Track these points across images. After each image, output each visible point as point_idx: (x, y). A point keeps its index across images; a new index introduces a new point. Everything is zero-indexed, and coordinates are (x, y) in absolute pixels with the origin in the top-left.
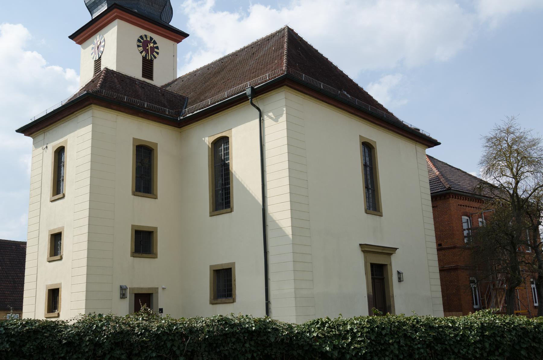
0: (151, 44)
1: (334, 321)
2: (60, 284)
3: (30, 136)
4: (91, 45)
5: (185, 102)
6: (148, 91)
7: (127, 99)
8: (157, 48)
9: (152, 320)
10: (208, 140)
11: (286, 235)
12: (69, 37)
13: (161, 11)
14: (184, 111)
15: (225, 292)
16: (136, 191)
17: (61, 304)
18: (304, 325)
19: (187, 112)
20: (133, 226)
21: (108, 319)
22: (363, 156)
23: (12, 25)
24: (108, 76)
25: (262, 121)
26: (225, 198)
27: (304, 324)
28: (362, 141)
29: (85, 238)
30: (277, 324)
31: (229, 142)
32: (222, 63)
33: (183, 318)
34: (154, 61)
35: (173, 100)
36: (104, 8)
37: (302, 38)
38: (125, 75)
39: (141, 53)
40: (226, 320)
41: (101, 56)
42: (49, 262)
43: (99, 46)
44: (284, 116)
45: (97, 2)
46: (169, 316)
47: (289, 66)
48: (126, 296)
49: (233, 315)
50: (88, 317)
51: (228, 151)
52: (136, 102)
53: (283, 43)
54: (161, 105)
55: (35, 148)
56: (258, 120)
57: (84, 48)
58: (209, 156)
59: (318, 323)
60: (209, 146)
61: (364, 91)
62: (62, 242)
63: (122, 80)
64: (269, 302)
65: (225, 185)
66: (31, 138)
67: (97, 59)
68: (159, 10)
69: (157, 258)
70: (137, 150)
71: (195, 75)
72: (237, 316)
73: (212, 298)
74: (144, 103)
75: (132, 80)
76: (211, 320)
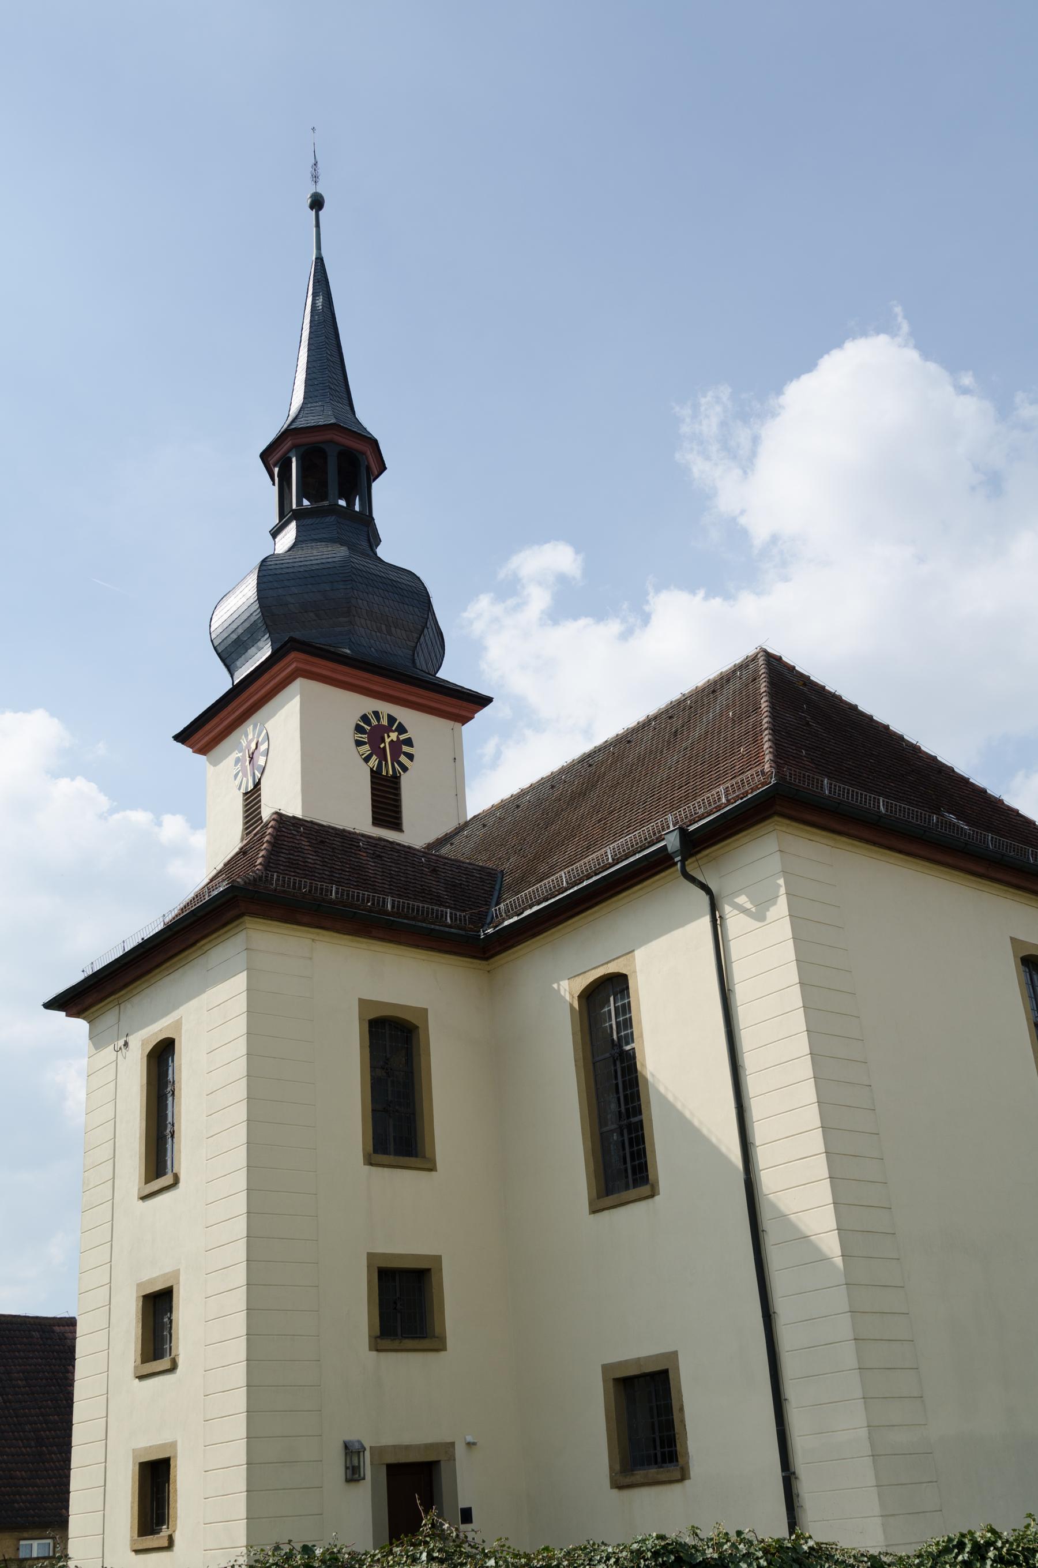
0: (391, 734)
1: (1011, 1539)
2: (173, 1445)
3: (84, 1015)
4: (231, 753)
5: (495, 885)
6: (393, 865)
7: (337, 893)
8: (409, 742)
9: (459, 1559)
10: (569, 987)
11: (826, 1259)
12: (173, 737)
13: (413, 644)
14: (496, 910)
15: (655, 1449)
16: (376, 1151)
17: (175, 1508)
18: (918, 1557)
19: (503, 914)
20: (371, 1256)
21: (329, 1560)
22: (1028, 999)
23: (20, 715)
24: (283, 834)
25: (718, 922)
26: (632, 1154)
27: (917, 1553)
28: (1022, 955)
29: (239, 1300)
30: (836, 1557)
31: (628, 988)
32: (590, 765)
33: (546, 1549)
34: (402, 778)
35: (461, 884)
36: (263, 652)
37: (808, 678)
38: (329, 827)
39: (367, 760)
40: (678, 1552)
41: (260, 780)
42: (141, 1378)
43: (253, 753)
44: (782, 902)
45: (245, 639)
46: (507, 1545)
47: (781, 759)
48: (362, 1475)
49: (698, 1531)
50: (274, 1555)
51: (628, 1016)
52: (363, 900)
53: (757, 694)
54: (431, 899)
55: (96, 1050)
56: (706, 921)
57: (215, 763)
58: (573, 1034)
59: (961, 1546)
60: (571, 1006)
61: (1008, 807)
62: (174, 1317)
63: (322, 842)
64: (794, 1473)
66: (85, 1022)
67: (249, 790)
68: (408, 642)
69: (444, 1349)
70: (370, 1032)
71: (518, 806)
72: (711, 1535)
73: (618, 1467)
74: (384, 898)
75: (347, 838)
76: (632, 1552)
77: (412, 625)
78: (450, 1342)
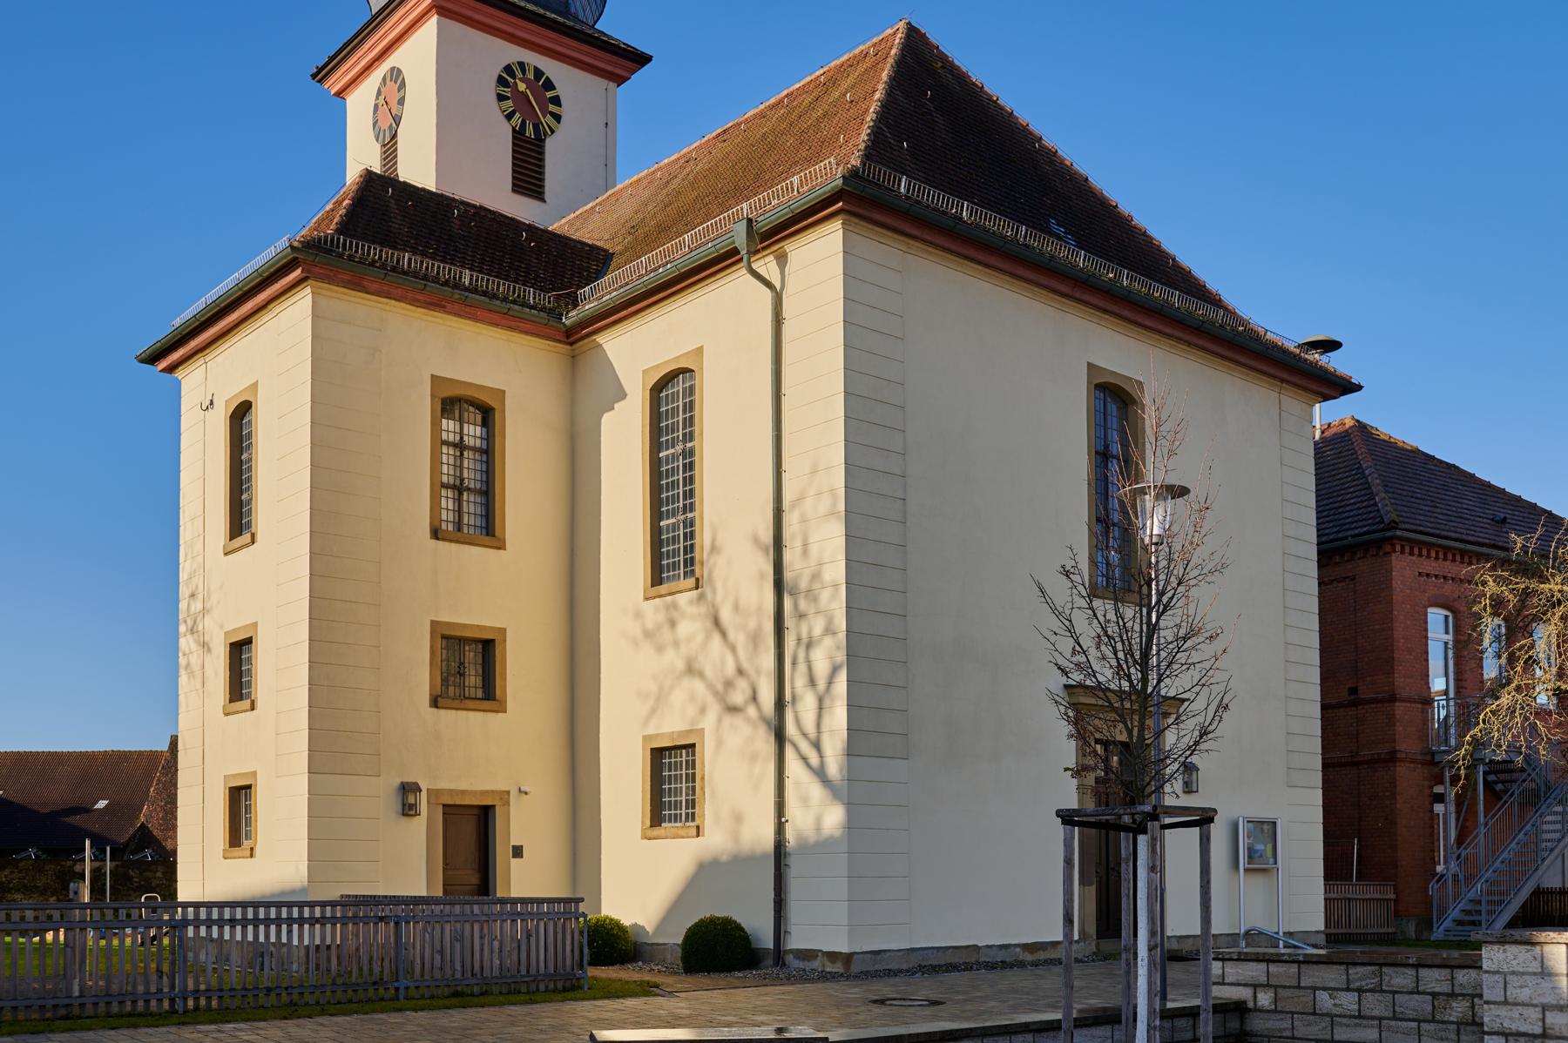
14: (581, 293)
42: (226, 714)
78: (510, 703)
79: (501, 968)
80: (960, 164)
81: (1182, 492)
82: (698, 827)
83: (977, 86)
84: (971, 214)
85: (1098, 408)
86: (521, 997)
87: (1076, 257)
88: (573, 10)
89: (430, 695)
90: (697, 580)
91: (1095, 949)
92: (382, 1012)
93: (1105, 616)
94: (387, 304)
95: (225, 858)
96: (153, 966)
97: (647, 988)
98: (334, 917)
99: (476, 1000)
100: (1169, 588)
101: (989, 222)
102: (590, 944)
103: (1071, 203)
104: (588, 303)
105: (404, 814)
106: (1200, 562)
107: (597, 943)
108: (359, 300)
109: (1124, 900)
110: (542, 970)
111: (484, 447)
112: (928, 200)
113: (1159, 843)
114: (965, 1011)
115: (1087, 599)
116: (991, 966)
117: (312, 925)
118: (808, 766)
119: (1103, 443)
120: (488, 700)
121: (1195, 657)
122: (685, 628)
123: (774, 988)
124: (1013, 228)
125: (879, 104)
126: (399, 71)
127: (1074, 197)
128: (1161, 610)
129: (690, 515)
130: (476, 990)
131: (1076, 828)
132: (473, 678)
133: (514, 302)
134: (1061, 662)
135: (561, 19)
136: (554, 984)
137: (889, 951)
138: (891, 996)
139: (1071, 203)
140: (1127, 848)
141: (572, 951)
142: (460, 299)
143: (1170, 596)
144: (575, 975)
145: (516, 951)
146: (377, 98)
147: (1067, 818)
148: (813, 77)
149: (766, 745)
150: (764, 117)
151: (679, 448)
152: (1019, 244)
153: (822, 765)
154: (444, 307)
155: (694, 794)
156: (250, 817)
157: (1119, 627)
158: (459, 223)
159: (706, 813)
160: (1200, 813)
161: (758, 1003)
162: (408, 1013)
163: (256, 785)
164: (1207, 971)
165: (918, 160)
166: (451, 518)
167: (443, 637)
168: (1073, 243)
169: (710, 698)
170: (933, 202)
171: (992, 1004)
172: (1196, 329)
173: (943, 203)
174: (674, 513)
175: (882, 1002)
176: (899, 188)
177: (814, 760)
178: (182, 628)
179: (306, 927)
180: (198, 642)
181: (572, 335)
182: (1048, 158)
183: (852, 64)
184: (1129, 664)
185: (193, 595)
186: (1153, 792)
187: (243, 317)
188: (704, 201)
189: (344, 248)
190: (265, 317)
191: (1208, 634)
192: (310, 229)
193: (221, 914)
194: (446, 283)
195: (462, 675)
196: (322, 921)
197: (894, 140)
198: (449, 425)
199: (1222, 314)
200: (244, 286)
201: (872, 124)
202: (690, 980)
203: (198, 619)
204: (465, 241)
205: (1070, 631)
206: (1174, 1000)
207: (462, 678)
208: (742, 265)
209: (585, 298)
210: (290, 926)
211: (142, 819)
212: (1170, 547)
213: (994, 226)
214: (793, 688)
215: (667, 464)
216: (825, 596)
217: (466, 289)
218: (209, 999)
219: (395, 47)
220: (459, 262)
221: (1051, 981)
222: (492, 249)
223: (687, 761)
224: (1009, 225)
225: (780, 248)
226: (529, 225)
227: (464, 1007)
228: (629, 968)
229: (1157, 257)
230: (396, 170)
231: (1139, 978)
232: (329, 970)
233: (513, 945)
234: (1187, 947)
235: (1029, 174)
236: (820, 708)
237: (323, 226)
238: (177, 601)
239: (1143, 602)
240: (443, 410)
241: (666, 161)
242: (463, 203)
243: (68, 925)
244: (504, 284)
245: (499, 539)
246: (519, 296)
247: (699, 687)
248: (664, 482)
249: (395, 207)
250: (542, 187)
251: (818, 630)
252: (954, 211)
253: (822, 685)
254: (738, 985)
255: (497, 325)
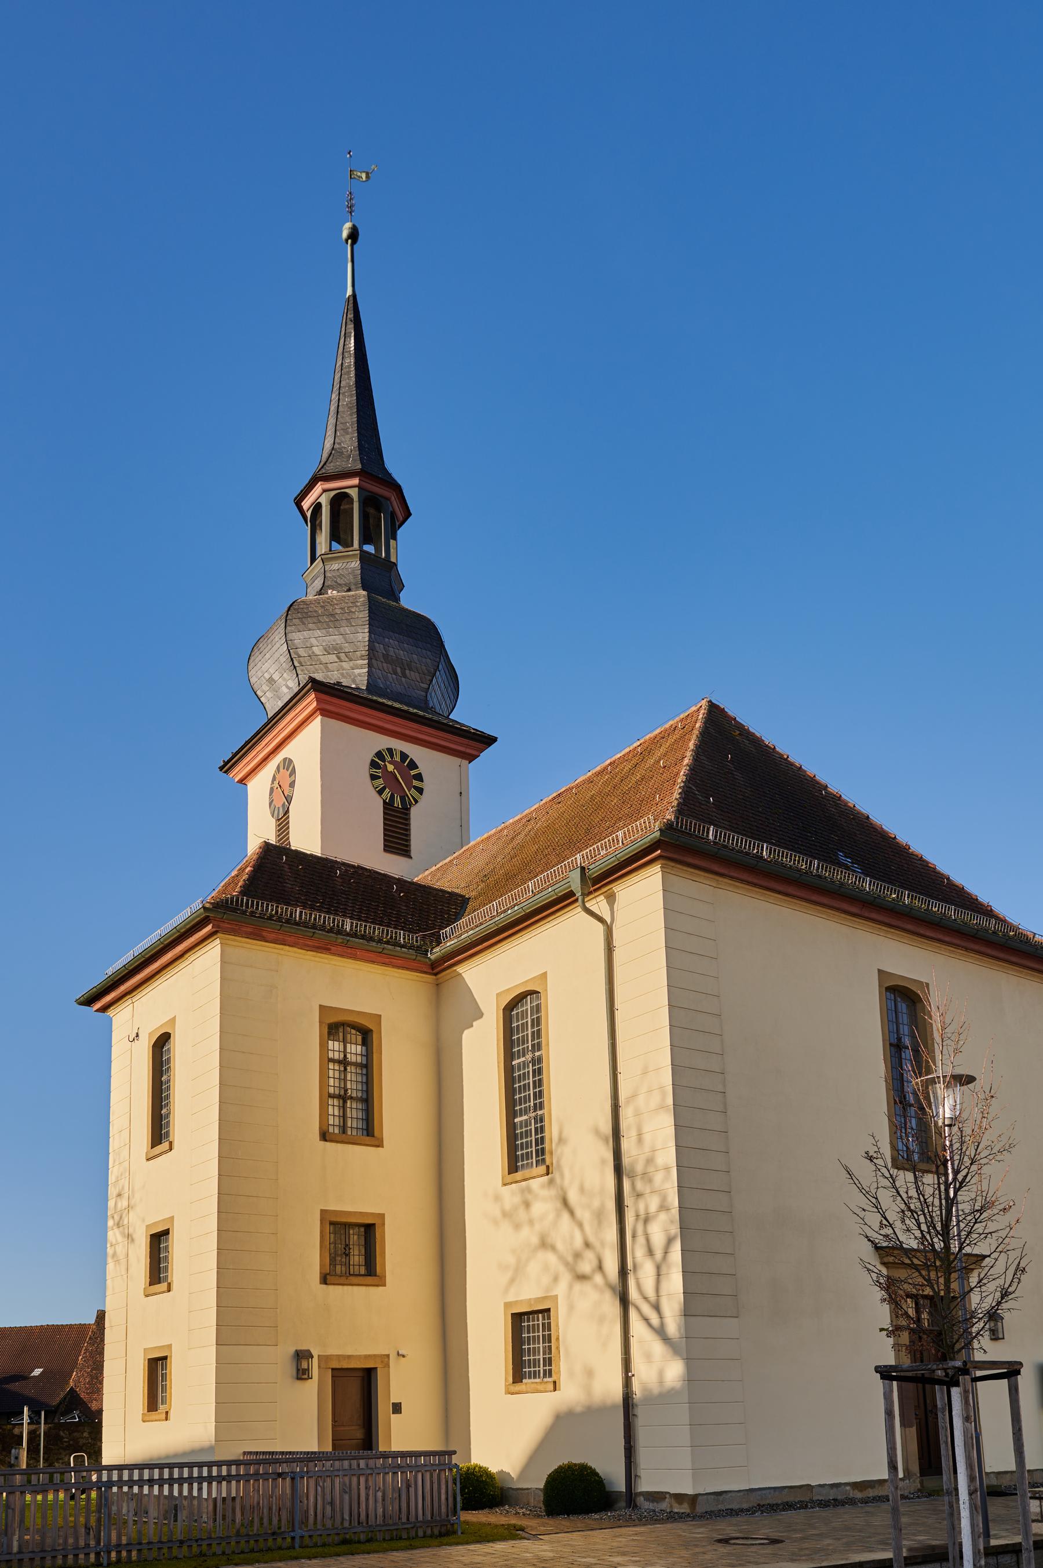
14: (443, 933)
42: (147, 1296)
65: (535, 1110)
77: (425, 668)
79: (384, 1516)
80: (758, 812)
81: (970, 1079)
82: (555, 1382)
83: (770, 748)
84: (770, 853)
85: (891, 1030)
86: (402, 1543)
87: (863, 882)
88: (431, 705)
89: (320, 1273)
90: (548, 1167)
91: (919, 1487)
92: (280, 1561)
93: (907, 1193)
94: (282, 949)
95: (144, 1421)
96: (82, 1520)
97: (514, 1532)
98: (238, 1475)
99: (362, 1547)
100: (963, 1167)
101: (786, 858)
102: (462, 1490)
103: (855, 838)
104: (450, 941)
105: (299, 1379)
106: (990, 1143)
107: (468, 1488)
108: (260, 948)
109: (943, 1446)
110: (420, 1518)
111: (364, 1062)
112: (732, 844)
113: (971, 1395)
114: (802, 1549)
115: (890, 1179)
116: (824, 1504)
117: (219, 1483)
118: (650, 1325)
119: (896, 1037)
120: (370, 1276)
121: (992, 1227)
122: (539, 1208)
123: (628, 1529)
124: (807, 861)
125: (688, 768)
126: (291, 761)
127: (858, 832)
128: (957, 1186)
129: (539, 1113)
130: (362, 1537)
131: (895, 1383)
132: (356, 1258)
133: (387, 943)
134: (870, 1233)
135: (421, 713)
136: (432, 1529)
137: (730, 1491)
138: (734, 1535)
139: (855, 838)
140: (942, 1399)
141: (447, 1499)
142: (342, 943)
143: (964, 1174)
144: (449, 1521)
145: (397, 1501)
146: (273, 783)
147: (885, 1373)
148: (631, 748)
149: (612, 1307)
150: (592, 782)
151: (529, 1056)
152: (812, 875)
153: (662, 1325)
154: (329, 949)
155: (550, 1353)
156: (166, 1373)
157: (921, 1202)
158: (341, 881)
159: (561, 1369)
160: (1007, 1367)
161: (615, 1544)
162: (303, 1560)
163: (171, 1356)
164: (1025, 1511)
165: (722, 811)
166: (337, 1123)
167: (331, 1223)
168: (860, 871)
169: (561, 1268)
170: (737, 845)
171: (828, 1541)
172: (972, 936)
173: (746, 845)
174: (526, 1111)
175: (725, 1541)
176: (708, 836)
177: (655, 1320)
178: (110, 1223)
179: (214, 1484)
180: (123, 1234)
181: (436, 967)
182: (834, 802)
183: (663, 736)
184: (932, 1234)
185: (119, 1195)
186: (963, 1348)
187: (164, 965)
188: (544, 853)
189: (247, 907)
190: (182, 965)
191: (1001, 1207)
192: (218, 892)
193: (141, 1475)
194: (331, 931)
195: (347, 1255)
196: (228, 1478)
197: (702, 796)
198: (334, 1046)
199: (994, 922)
200: (165, 940)
201: (682, 785)
202: (551, 1523)
203: (124, 1216)
204: (346, 895)
205: (877, 1208)
206: (997, 1537)
207: (348, 1258)
208: (577, 904)
209: (446, 936)
210: (200, 1484)
211: (72, 1384)
212: (962, 1131)
213: (790, 862)
214: (633, 1258)
215: (519, 1070)
216: (658, 1177)
217: (348, 935)
218: (129, 1552)
219: (287, 742)
220: (342, 912)
221: (880, 1518)
222: (368, 900)
223: (543, 1324)
224: (803, 860)
225: (609, 890)
226: (399, 879)
227: (353, 1554)
228: (496, 1512)
229: (934, 878)
230: (288, 838)
231: (962, 1520)
232: (234, 1521)
233: (395, 1496)
234: (1005, 1482)
235: (818, 816)
236: (659, 1275)
237: (229, 889)
238: (106, 1200)
239: (939, 1165)
240: (329, 1033)
241: (511, 821)
242: (344, 864)
243: (10, 1489)
244: (379, 929)
245: (378, 1139)
246: (391, 937)
247: (551, 1258)
248: (517, 1085)
249: (289, 870)
250: (408, 846)
251: (653, 1206)
252: (755, 851)
253: (659, 1254)
254: (595, 1527)
255: (373, 962)
